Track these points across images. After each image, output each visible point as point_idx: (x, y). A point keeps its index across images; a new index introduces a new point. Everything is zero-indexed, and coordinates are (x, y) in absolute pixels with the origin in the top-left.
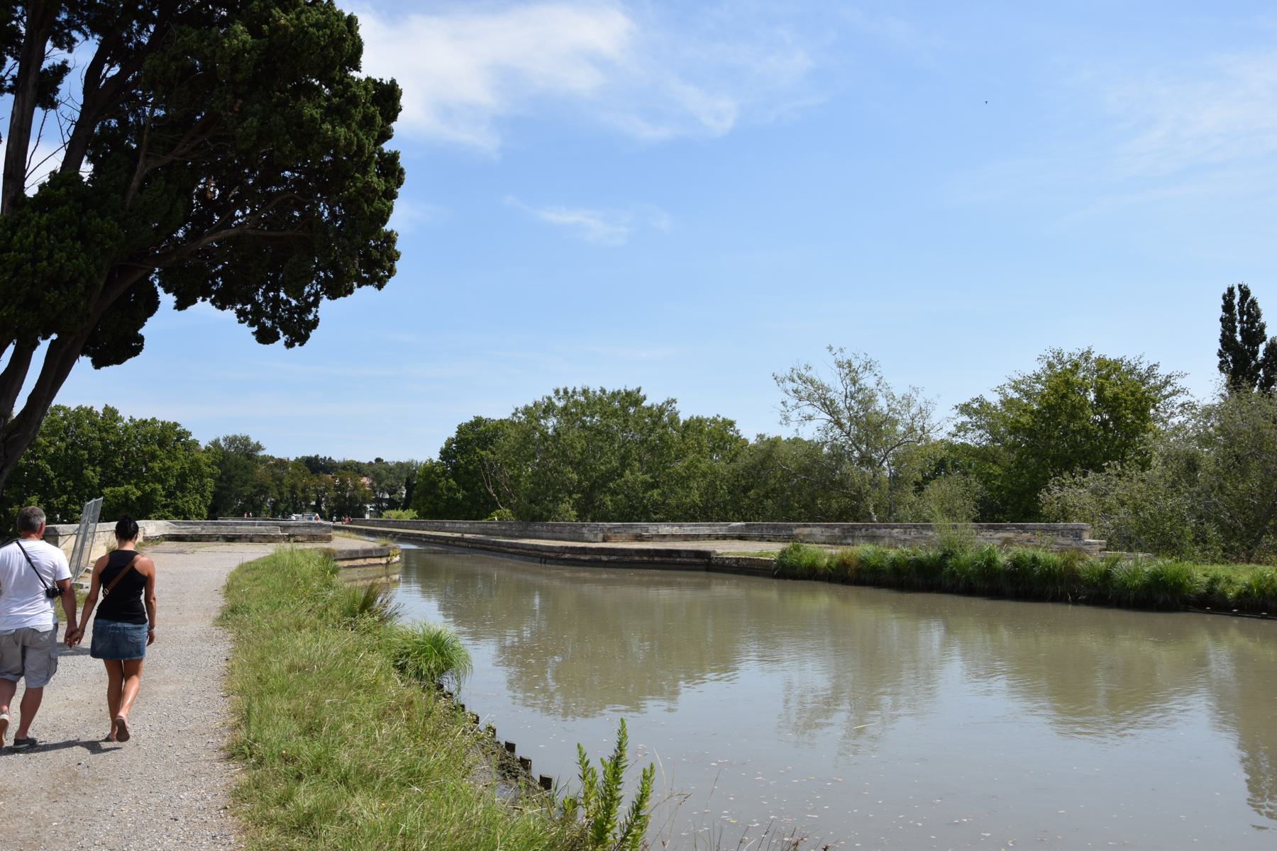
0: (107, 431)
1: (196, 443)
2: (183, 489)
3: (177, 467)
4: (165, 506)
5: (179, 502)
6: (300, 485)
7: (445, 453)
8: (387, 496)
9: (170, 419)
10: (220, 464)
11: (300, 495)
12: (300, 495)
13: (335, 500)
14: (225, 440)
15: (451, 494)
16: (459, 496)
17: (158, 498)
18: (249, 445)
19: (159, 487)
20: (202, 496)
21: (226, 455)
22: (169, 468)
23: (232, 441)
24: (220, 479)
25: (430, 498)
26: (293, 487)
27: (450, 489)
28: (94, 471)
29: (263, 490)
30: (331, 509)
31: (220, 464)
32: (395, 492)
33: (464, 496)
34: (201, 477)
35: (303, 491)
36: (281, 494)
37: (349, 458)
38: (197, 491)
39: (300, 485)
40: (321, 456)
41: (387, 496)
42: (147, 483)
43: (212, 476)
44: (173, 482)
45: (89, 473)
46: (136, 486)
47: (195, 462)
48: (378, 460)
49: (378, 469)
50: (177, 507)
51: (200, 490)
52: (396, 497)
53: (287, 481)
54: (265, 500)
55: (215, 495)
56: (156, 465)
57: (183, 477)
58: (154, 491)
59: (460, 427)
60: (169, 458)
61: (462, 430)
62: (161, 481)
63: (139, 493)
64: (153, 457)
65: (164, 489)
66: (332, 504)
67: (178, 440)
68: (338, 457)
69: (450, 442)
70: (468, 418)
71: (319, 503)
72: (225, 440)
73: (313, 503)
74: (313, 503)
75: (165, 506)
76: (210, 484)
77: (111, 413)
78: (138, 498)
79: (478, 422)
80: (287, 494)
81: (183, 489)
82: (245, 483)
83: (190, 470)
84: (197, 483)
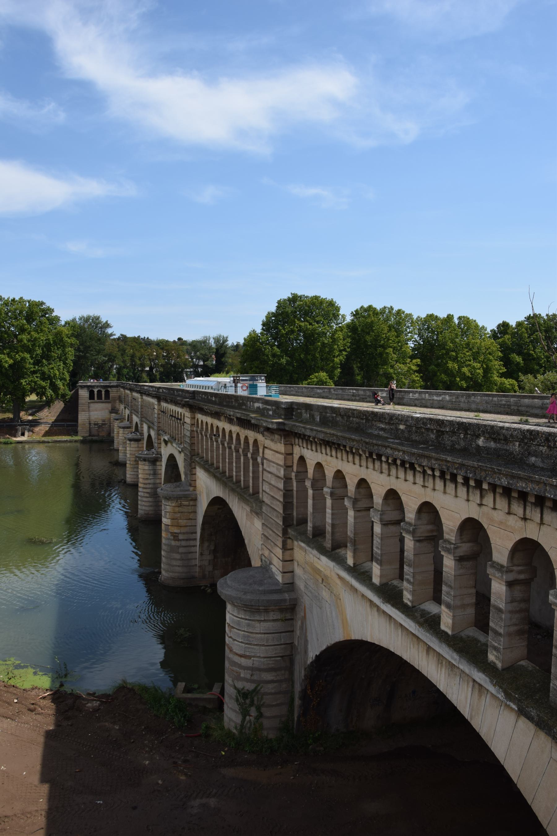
1: (57, 319)
3: (43, 338)
4: (34, 372)
5: (46, 369)
6: (138, 354)
7: (266, 325)
9: (36, 298)
11: (138, 362)
15: (276, 360)
16: (284, 361)
17: (28, 366)
18: (100, 323)
19: (27, 356)
20: (65, 363)
21: (81, 328)
22: (36, 339)
23: (87, 319)
24: (78, 350)
25: (256, 363)
26: (133, 356)
27: (274, 355)
29: (112, 359)
30: (161, 373)
31: (77, 336)
32: (207, 360)
33: (287, 361)
34: (64, 346)
36: (124, 362)
38: (60, 358)
39: (138, 354)
40: (142, 337)
41: (201, 363)
42: (17, 353)
43: (72, 345)
44: (39, 351)
46: (8, 354)
47: (58, 334)
48: (180, 339)
50: (43, 373)
51: (63, 358)
52: (208, 363)
54: (112, 366)
55: (74, 362)
56: (24, 337)
57: (48, 346)
58: (23, 359)
59: (279, 302)
60: (36, 331)
61: (281, 304)
62: (30, 351)
64: (22, 330)
65: (32, 358)
68: (154, 337)
69: (269, 316)
70: (286, 295)
72: (80, 319)
73: (147, 369)
74: (147, 369)
75: (34, 372)
76: (71, 353)
78: (10, 366)
79: (294, 298)
81: (48, 358)
83: (54, 342)
84: (59, 352)
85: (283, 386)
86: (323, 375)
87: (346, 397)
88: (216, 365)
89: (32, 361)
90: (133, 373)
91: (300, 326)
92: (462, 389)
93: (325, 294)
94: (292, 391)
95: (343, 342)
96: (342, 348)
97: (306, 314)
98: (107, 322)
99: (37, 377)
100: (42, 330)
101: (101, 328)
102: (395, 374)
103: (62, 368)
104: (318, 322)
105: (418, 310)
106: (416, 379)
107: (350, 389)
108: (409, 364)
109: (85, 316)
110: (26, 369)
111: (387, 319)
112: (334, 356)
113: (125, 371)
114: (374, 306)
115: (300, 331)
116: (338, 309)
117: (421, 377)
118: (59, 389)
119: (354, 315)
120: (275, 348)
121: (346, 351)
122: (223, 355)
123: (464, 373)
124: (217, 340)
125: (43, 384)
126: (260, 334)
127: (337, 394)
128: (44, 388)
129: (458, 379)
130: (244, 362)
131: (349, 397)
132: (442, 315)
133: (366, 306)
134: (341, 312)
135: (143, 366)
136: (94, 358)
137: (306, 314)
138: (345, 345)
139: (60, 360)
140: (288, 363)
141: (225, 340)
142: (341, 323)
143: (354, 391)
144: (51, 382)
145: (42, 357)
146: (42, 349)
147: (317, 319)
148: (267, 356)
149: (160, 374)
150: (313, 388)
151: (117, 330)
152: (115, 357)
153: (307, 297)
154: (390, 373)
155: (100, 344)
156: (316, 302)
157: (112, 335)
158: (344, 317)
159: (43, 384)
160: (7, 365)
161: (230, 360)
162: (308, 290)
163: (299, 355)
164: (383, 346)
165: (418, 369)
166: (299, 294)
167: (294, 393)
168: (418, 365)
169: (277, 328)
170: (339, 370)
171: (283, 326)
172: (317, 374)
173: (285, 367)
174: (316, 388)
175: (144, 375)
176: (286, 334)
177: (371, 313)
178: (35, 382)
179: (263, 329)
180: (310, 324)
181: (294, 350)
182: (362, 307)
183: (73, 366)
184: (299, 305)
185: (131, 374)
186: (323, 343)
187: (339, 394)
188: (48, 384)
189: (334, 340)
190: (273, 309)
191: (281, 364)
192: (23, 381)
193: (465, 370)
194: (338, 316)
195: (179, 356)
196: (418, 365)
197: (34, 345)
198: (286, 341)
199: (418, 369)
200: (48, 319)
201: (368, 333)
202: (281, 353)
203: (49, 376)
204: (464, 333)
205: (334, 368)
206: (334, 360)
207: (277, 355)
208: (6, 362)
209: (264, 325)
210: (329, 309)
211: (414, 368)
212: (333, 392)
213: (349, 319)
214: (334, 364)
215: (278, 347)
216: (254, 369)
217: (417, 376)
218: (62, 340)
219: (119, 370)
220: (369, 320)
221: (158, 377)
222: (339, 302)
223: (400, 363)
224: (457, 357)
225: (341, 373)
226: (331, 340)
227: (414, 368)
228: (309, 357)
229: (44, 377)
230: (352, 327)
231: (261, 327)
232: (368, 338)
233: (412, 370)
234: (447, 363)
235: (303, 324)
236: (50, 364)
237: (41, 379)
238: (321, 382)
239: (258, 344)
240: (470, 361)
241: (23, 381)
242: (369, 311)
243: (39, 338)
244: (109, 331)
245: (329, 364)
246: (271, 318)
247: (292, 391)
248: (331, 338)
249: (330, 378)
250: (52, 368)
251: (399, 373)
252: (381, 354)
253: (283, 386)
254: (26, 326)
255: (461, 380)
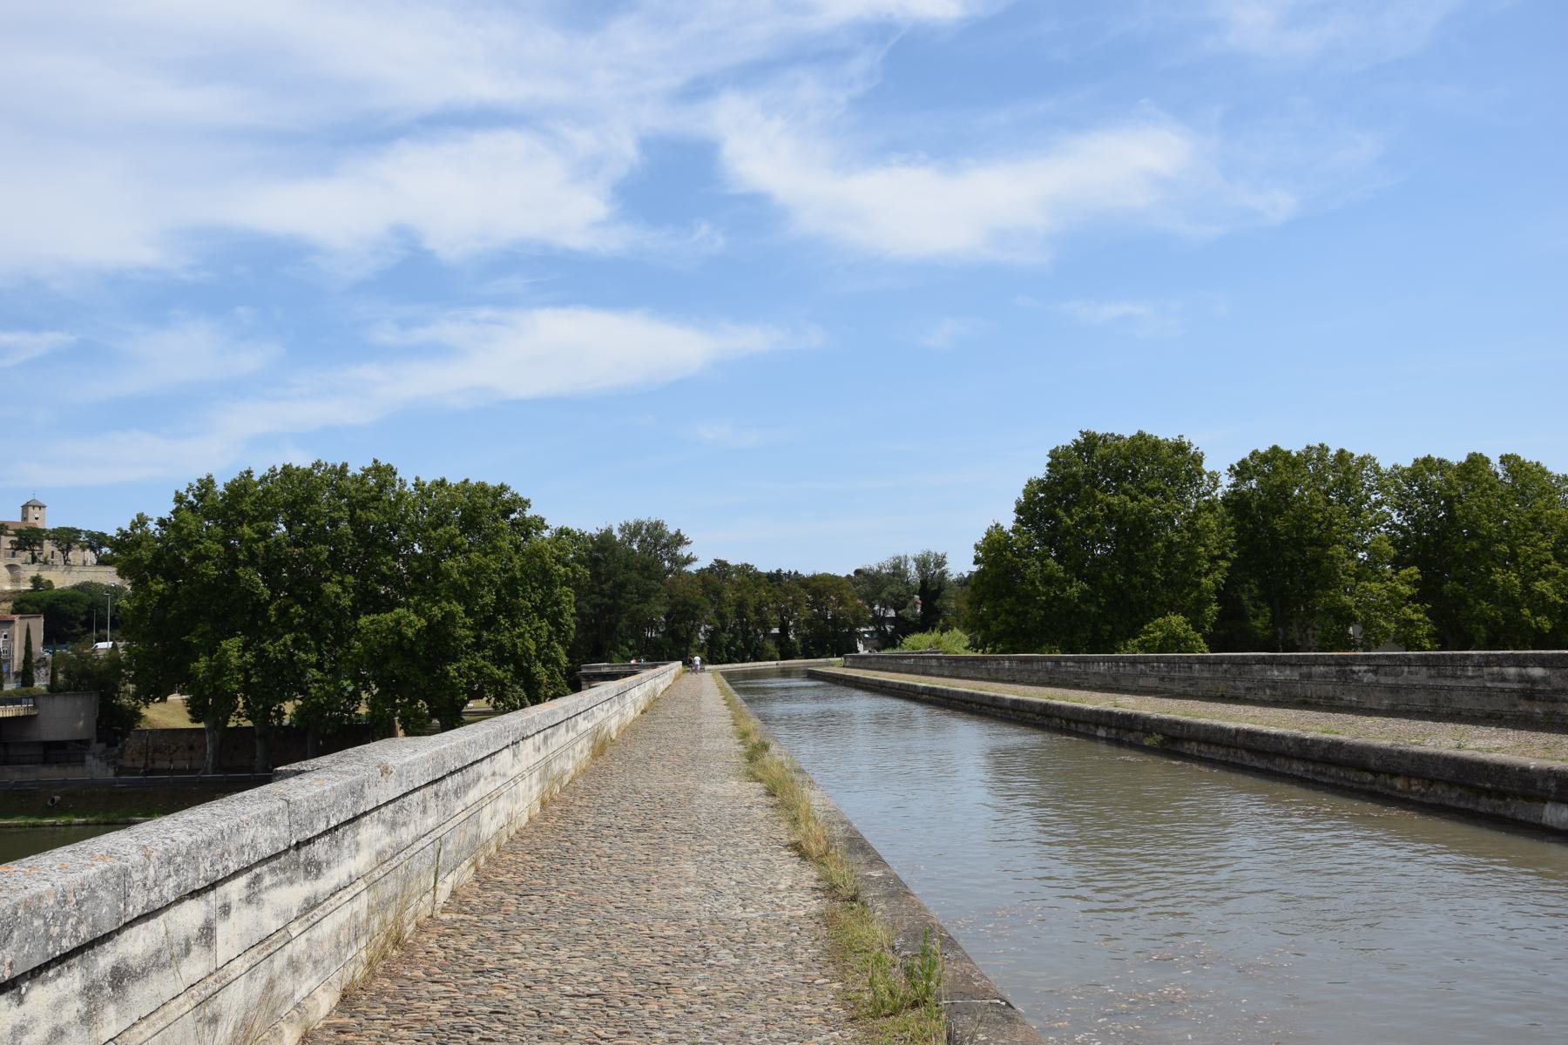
0: (364, 507)
2: (511, 613)
5: (505, 638)
6: (752, 601)
7: (1025, 510)
8: (892, 613)
10: (593, 563)
12: (754, 617)
13: (809, 623)
14: (622, 530)
15: (1053, 591)
18: (661, 536)
19: (458, 608)
23: (634, 531)
25: (1008, 602)
27: (1049, 580)
28: (341, 583)
30: (805, 639)
31: (593, 563)
32: (904, 605)
35: (758, 611)
36: (721, 616)
37: (820, 571)
38: (540, 610)
39: (752, 601)
41: (892, 613)
44: (489, 598)
45: (331, 588)
49: (869, 583)
50: (500, 648)
51: (548, 610)
52: (907, 612)
53: (729, 595)
58: (449, 617)
61: (1058, 459)
62: (465, 597)
63: (424, 622)
66: (806, 631)
67: (505, 515)
69: (1032, 489)
70: (1068, 437)
71: (784, 629)
74: (776, 630)
75: (478, 645)
77: (383, 474)
79: (1089, 443)
80: (732, 622)
82: (645, 596)
85: (1104, 660)
86: (1177, 621)
87: (1467, 702)
88: (923, 617)
89: (469, 621)
90: (744, 641)
91: (1108, 505)
92: (1541, 640)
93: (1165, 432)
94: (1143, 674)
95: (1218, 534)
96: (1216, 553)
97: (1120, 476)
98: (678, 533)
99: (484, 658)
100: (496, 549)
101: (665, 546)
102: (1357, 607)
103: (545, 634)
104: (1152, 493)
105: (1394, 452)
106: (1415, 617)
107: (1501, 662)
108: (1390, 579)
109: (631, 522)
110: (455, 639)
111: (1319, 477)
112: (1199, 574)
113: (725, 637)
114: (1285, 447)
115: (1108, 519)
116: (1198, 459)
117: (1428, 613)
118: (540, 683)
119: (1237, 473)
120: (1050, 561)
121: (1228, 559)
122: (937, 594)
123: (1543, 595)
124: (923, 563)
125: (499, 673)
126: (1013, 531)
127: (1394, 689)
128: (501, 682)
129: (1526, 612)
130: (980, 603)
131: (1501, 705)
132: (1457, 456)
133: (1263, 448)
134: (1207, 466)
135: (766, 626)
136: (635, 607)
137: (1120, 476)
138: (1222, 545)
139: (541, 618)
140: (1084, 597)
141: (940, 562)
142: (1209, 493)
143: (1537, 672)
144: (518, 666)
145: (497, 611)
146: (498, 593)
147: (1150, 485)
148: (1033, 583)
149: (803, 641)
150: (1245, 662)
151: (704, 550)
152: (696, 607)
153: (1119, 438)
154: (1346, 607)
155: (650, 578)
156: (1144, 449)
157: (689, 561)
158: (1214, 477)
159: (499, 673)
160: (410, 633)
161: (953, 605)
162: (1122, 425)
163: (1112, 576)
164: (1314, 542)
165: (1415, 591)
166: (1099, 431)
167: (1152, 682)
168: (1416, 584)
169: (1054, 516)
170: (1214, 607)
171: (1067, 510)
172: (1160, 620)
173: (1077, 606)
174: (1262, 660)
175: (770, 645)
176: (1075, 526)
177: (1279, 463)
178: (479, 671)
179: (1018, 520)
180: (1133, 499)
181: (1101, 563)
182: (1254, 454)
183: (578, 631)
184: (1102, 457)
185: (739, 642)
186: (1170, 544)
187: (1412, 688)
188: (509, 675)
189: (1198, 535)
190: (1040, 472)
191: (1068, 600)
192: (451, 669)
193: (1541, 586)
194: (1200, 474)
195: (841, 602)
196: (1416, 584)
197: (476, 583)
198: (1076, 545)
199: (1415, 591)
200: (514, 524)
201: (1279, 512)
202: (1065, 571)
203: (514, 654)
204: (1521, 494)
205: (1201, 603)
206: (1199, 585)
207: (1058, 579)
208: (410, 624)
209: (1019, 511)
210: (1176, 463)
211: (1406, 590)
212: (1369, 678)
213: (1226, 482)
214: (1201, 593)
215: (1058, 559)
216: (1003, 617)
217: (1416, 611)
218: (545, 571)
219: (713, 637)
220: (1276, 481)
221: (799, 646)
222: (1197, 440)
223: (1369, 580)
224: (1513, 557)
225: (1220, 614)
226: (1187, 535)
227: (1406, 590)
228: (1137, 580)
229: (500, 659)
230: (1237, 504)
231: (1014, 516)
232: (1279, 524)
233: (1401, 596)
234: (1490, 572)
235: (1115, 500)
236: (515, 625)
237: (494, 661)
238: (1173, 642)
239: (1009, 555)
240: (1548, 562)
241: (451, 669)
242: (1274, 458)
243: (488, 566)
244: (684, 551)
245: (1188, 594)
246: (1036, 494)
247: (1143, 674)
248: (1188, 529)
249: (1197, 629)
250: (521, 635)
251: (1368, 605)
252: (1316, 562)
253: (1104, 660)
254: (458, 540)
255: (1534, 614)
